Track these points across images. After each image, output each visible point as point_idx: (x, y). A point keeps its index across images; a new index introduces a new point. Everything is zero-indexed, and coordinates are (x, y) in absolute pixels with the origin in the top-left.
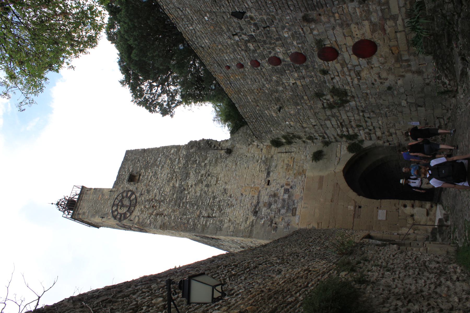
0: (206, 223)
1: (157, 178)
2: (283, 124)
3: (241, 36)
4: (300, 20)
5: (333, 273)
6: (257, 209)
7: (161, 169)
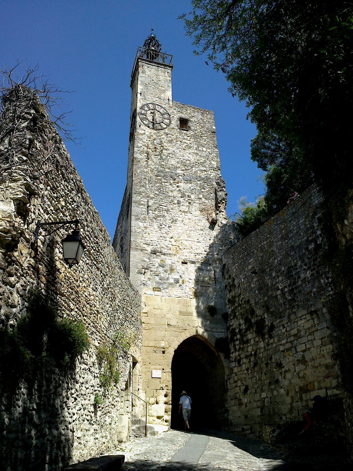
0: (142, 204)
1: (184, 149)
2: (241, 276)
3: (321, 236)
5: (97, 335)
6: (158, 254)
7: (194, 153)
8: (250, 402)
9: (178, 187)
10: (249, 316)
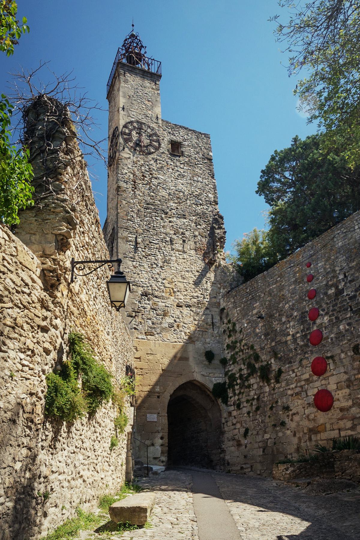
0: (130, 241)
2: (244, 321)
3: (343, 281)
4: (357, 341)
8: (251, 443)
9: (170, 222)
10: (253, 362)
